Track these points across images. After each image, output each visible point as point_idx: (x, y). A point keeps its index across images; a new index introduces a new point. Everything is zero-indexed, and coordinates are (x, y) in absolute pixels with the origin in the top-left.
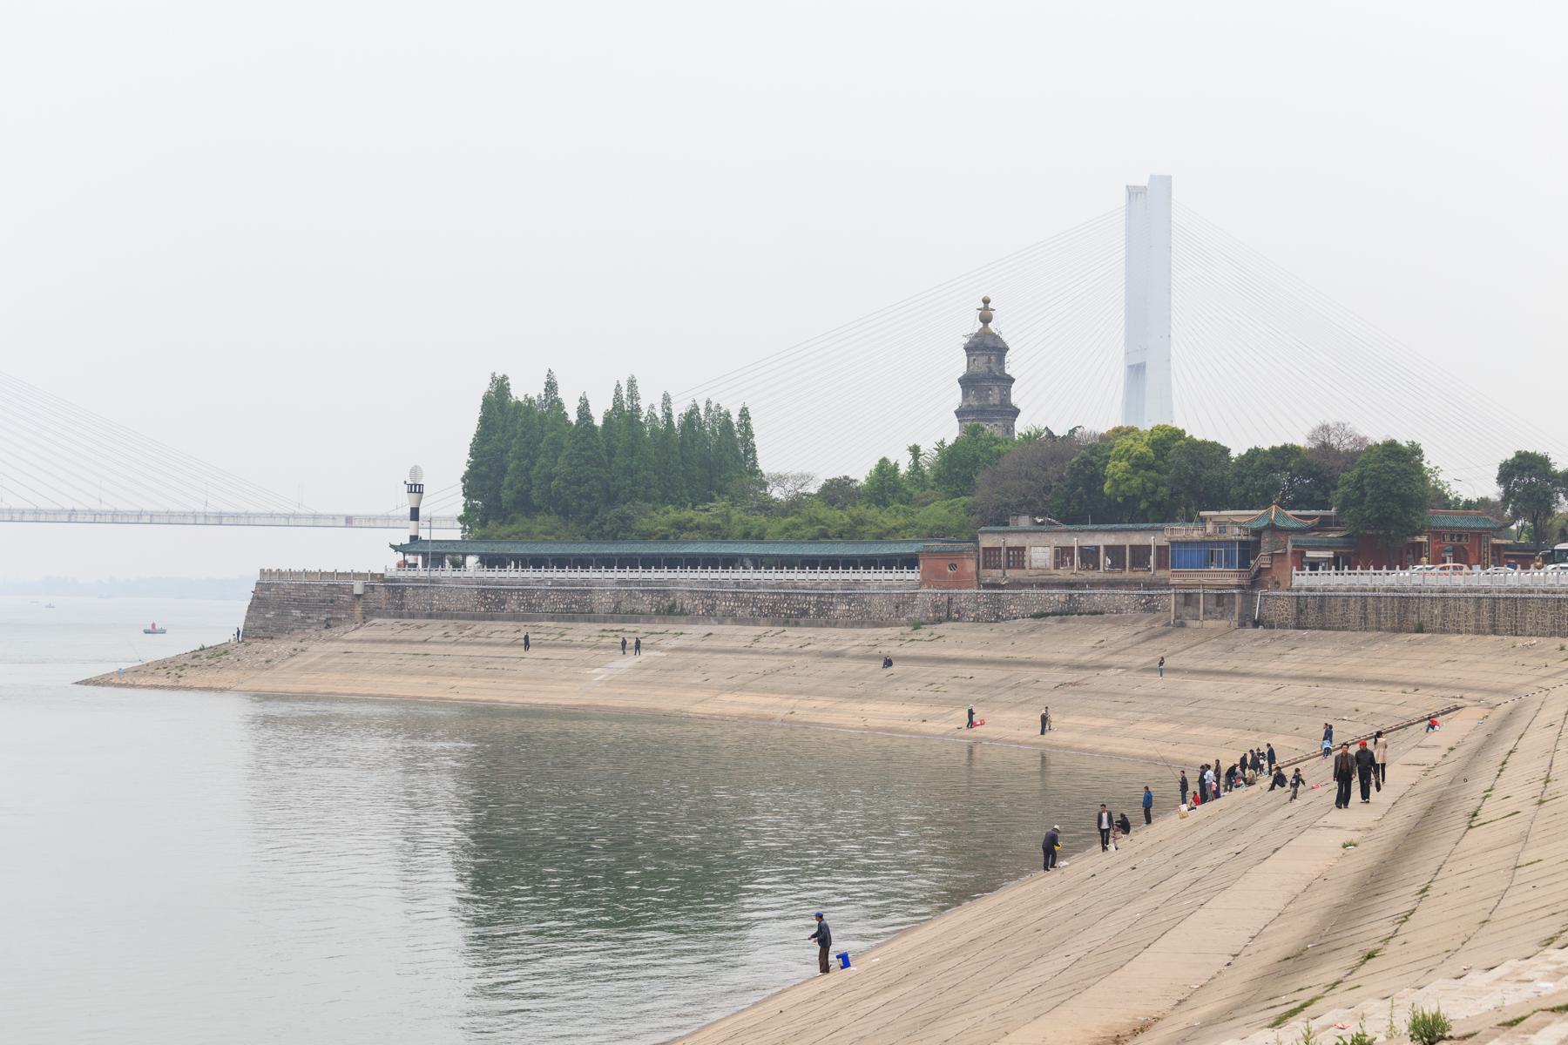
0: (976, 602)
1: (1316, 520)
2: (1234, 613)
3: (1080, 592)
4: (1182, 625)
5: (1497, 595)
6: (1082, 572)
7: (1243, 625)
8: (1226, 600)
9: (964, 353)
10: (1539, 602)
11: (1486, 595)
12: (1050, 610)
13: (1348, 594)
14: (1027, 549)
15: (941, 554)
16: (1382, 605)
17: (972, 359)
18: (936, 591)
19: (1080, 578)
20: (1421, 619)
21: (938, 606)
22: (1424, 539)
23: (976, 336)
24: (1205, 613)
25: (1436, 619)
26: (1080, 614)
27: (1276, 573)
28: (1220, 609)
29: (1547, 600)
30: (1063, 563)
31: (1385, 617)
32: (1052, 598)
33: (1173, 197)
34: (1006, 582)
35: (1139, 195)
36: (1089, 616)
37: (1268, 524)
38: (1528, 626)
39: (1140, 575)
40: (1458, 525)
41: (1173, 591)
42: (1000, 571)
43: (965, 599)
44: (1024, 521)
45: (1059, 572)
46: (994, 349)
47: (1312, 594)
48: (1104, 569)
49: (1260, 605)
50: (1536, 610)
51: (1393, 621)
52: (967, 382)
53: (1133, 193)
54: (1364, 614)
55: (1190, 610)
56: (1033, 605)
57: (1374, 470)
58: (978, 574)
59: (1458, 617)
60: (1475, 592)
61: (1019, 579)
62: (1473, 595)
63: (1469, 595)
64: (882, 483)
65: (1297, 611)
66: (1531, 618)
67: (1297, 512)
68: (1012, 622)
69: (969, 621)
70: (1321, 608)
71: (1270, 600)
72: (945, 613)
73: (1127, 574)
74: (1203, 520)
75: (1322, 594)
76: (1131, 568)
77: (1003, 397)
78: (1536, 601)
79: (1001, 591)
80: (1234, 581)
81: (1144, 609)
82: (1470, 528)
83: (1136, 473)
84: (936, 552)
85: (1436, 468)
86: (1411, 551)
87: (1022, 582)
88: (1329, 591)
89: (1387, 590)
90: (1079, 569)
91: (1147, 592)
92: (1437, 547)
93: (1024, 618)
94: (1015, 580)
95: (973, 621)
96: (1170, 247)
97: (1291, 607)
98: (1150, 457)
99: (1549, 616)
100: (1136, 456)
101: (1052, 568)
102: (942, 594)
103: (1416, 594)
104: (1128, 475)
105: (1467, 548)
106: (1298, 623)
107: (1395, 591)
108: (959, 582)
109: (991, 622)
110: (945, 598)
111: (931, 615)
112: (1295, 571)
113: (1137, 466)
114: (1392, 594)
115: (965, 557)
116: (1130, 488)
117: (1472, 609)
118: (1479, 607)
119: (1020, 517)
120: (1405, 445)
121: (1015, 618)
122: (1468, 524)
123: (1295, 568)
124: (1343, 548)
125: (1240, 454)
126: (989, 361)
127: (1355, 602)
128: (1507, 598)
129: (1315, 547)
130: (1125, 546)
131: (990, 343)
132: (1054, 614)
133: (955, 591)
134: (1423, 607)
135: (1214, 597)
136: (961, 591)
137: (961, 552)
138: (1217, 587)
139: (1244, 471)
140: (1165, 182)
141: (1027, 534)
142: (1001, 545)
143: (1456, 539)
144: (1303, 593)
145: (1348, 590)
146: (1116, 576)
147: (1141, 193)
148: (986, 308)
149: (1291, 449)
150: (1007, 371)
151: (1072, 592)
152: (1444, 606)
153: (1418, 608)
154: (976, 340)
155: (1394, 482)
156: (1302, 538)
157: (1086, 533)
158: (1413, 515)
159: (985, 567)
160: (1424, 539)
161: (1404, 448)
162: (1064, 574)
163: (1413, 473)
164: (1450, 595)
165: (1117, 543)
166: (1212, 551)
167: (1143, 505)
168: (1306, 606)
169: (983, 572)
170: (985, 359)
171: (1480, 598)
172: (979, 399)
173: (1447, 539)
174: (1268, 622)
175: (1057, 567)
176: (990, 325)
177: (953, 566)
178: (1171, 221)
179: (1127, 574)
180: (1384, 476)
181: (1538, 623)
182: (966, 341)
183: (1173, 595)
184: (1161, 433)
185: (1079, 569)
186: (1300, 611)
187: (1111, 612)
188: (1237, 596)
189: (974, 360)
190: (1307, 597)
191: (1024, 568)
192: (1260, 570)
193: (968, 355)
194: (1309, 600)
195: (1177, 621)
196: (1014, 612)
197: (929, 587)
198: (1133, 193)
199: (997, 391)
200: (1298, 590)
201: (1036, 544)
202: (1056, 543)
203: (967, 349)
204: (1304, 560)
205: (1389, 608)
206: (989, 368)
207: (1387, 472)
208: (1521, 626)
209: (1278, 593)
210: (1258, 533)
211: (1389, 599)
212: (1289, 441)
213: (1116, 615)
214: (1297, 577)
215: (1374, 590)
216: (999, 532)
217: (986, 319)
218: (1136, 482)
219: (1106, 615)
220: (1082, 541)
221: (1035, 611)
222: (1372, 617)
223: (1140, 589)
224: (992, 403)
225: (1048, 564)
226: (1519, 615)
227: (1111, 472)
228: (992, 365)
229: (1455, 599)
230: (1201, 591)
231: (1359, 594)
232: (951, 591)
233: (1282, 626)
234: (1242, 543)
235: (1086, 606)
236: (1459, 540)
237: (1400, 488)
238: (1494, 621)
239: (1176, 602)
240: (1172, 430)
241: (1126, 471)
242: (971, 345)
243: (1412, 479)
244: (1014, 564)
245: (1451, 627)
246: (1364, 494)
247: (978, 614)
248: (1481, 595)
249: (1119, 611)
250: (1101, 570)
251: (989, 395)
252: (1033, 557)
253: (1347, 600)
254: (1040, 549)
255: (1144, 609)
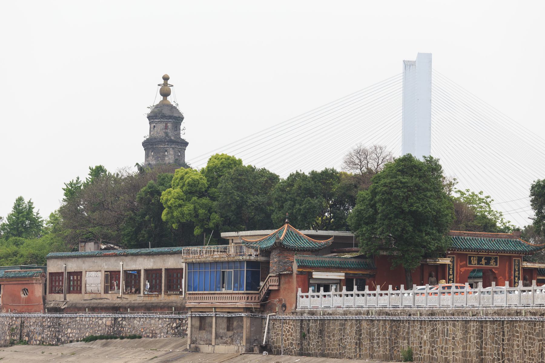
0: (42, 326)
1: (330, 240)
2: (242, 337)
3: (123, 316)
4: (197, 350)
5: (484, 318)
6: (126, 296)
7: (250, 351)
8: (235, 323)
9: (147, 121)
10: (527, 326)
11: (473, 318)
12: (98, 334)
13: (344, 317)
14: (83, 274)
15: (16, 279)
16: (375, 330)
17: (153, 125)
18: (12, 315)
19: (125, 301)
20: (411, 346)
21: (13, 329)
22: (447, 261)
23: (157, 107)
24: (217, 337)
25: (425, 345)
26: (122, 338)
27: (282, 295)
28: (230, 333)
29: (534, 323)
30: (111, 288)
31: (378, 343)
32: (100, 322)
33: (432, 68)
34: (66, 306)
35: (412, 66)
36: (129, 340)
37: (275, 243)
38: (515, 354)
39: (173, 298)
40: (486, 247)
41: (189, 314)
42: (62, 295)
43: (34, 323)
44: (90, 247)
45: (108, 296)
46: (170, 117)
47: (313, 317)
48: (144, 294)
49: (269, 329)
50: (523, 336)
51: (385, 347)
52: (148, 145)
53: (408, 65)
54: (359, 339)
55: (204, 334)
56: (86, 329)
57: (385, 185)
58: (44, 299)
59: (446, 344)
60: (463, 314)
61: (76, 303)
62: (461, 318)
63: (456, 318)
64: (18, 218)
65: (301, 336)
66: (518, 346)
67: (312, 232)
68: (68, 345)
69: (36, 344)
70: (321, 332)
71: (278, 324)
72: (18, 336)
73: (163, 298)
74: (225, 241)
75: (322, 318)
76: (166, 292)
77: (177, 157)
78: (523, 324)
79: (61, 315)
80: (242, 304)
81: (175, 334)
82: (498, 251)
83: (188, 199)
84: (12, 277)
85: (488, 197)
86: (433, 273)
87: (78, 305)
88: (329, 314)
89: (380, 313)
90: (124, 293)
91: (177, 316)
92: (463, 270)
93: (78, 341)
94: (72, 304)
95: (39, 344)
96: (431, 100)
97: (296, 332)
98: (203, 184)
99: (537, 344)
100: (188, 183)
101: (103, 292)
102: (17, 318)
103: (406, 317)
104: (181, 202)
105: (496, 272)
106: (301, 349)
107: (387, 314)
108: (29, 306)
109: (53, 345)
110: (19, 322)
111: (8, 338)
112: (300, 293)
113: (190, 193)
114: (383, 317)
115: (34, 282)
116: (183, 214)
117: (459, 334)
118: (466, 332)
119: (87, 243)
120: (422, 160)
121: (71, 342)
122: (497, 247)
123: (300, 289)
124: (356, 269)
125: (279, 176)
126: (166, 127)
127: (351, 326)
128: (493, 322)
129: (325, 267)
130: (161, 270)
131: (167, 112)
132: (101, 337)
133: (26, 315)
134: (413, 331)
135: (225, 320)
136: (31, 315)
137: (31, 277)
138: (227, 310)
139: (284, 196)
140: (427, 58)
141: (84, 259)
142: (63, 270)
143: (483, 262)
144: (306, 316)
145: (345, 314)
146: (154, 300)
147: (413, 65)
148: (166, 84)
149: (332, 174)
150: (182, 137)
151: (117, 316)
152: (433, 330)
153: (408, 333)
154: (156, 110)
155: (407, 198)
156: (309, 258)
157: (130, 257)
158: (426, 234)
159: (51, 292)
160: (447, 261)
161: (421, 163)
162: (112, 298)
163: (428, 190)
164: (438, 318)
165: (155, 267)
166: (223, 272)
167: (197, 231)
168: (309, 330)
169: (50, 297)
170: (162, 126)
171: (467, 322)
172: (157, 159)
173: (474, 261)
174: (276, 347)
175: (106, 292)
176: (169, 98)
177: (25, 291)
178: (431, 83)
179: (163, 298)
180: (395, 192)
181: (525, 351)
182: (149, 111)
183: (189, 319)
184: (216, 161)
185: (124, 293)
186: (303, 336)
187: (148, 336)
188: (245, 320)
189: (154, 126)
190: (309, 320)
191: (80, 292)
192: (269, 292)
193: (150, 123)
194: (311, 324)
195: (192, 345)
196: (71, 335)
197: (7, 311)
198: (408, 65)
199: (172, 152)
200: (302, 314)
201: (91, 269)
202: (106, 267)
203: (149, 117)
204: (311, 282)
205: (382, 332)
206: (166, 134)
207: (398, 188)
208: (508, 354)
209: (284, 316)
210: (266, 252)
211: (381, 322)
212: (329, 167)
213: (151, 339)
214: (301, 299)
215: (368, 313)
216: (61, 258)
217: (165, 93)
218: (188, 208)
219: (143, 339)
220: (127, 265)
221: (87, 335)
222: (366, 343)
223: (172, 313)
224: (167, 162)
225: (99, 289)
226: (506, 342)
227: (165, 198)
228: (168, 131)
229: (443, 322)
230: (213, 314)
231: (354, 317)
232: (23, 315)
233: (288, 352)
234: (250, 263)
235: (127, 330)
236: (487, 263)
237: (412, 205)
238: (481, 348)
239: (192, 326)
240: (228, 158)
241: (179, 198)
242: (152, 114)
243: (425, 196)
244: (74, 289)
245: (439, 355)
246: (376, 212)
247: (43, 338)
248: (469, 318)
249: (154, 335)
250: (142, 294)
251: (166, 155)
252: (88, 282)
253: (344, 325)
254: (93, 274)
255: (175, 334)
